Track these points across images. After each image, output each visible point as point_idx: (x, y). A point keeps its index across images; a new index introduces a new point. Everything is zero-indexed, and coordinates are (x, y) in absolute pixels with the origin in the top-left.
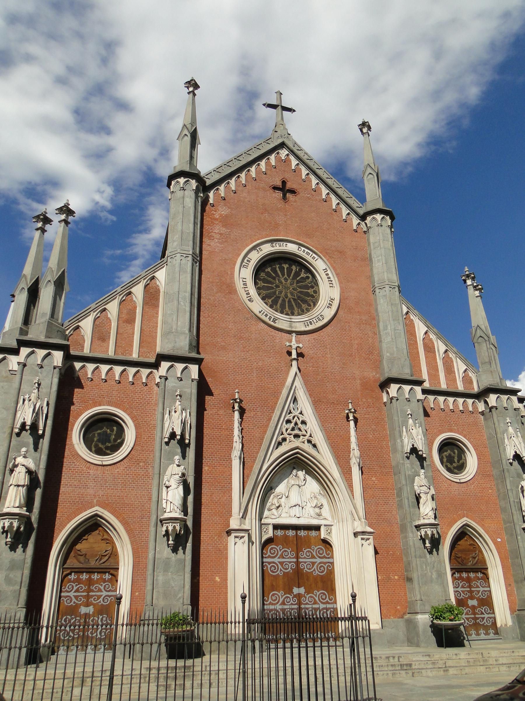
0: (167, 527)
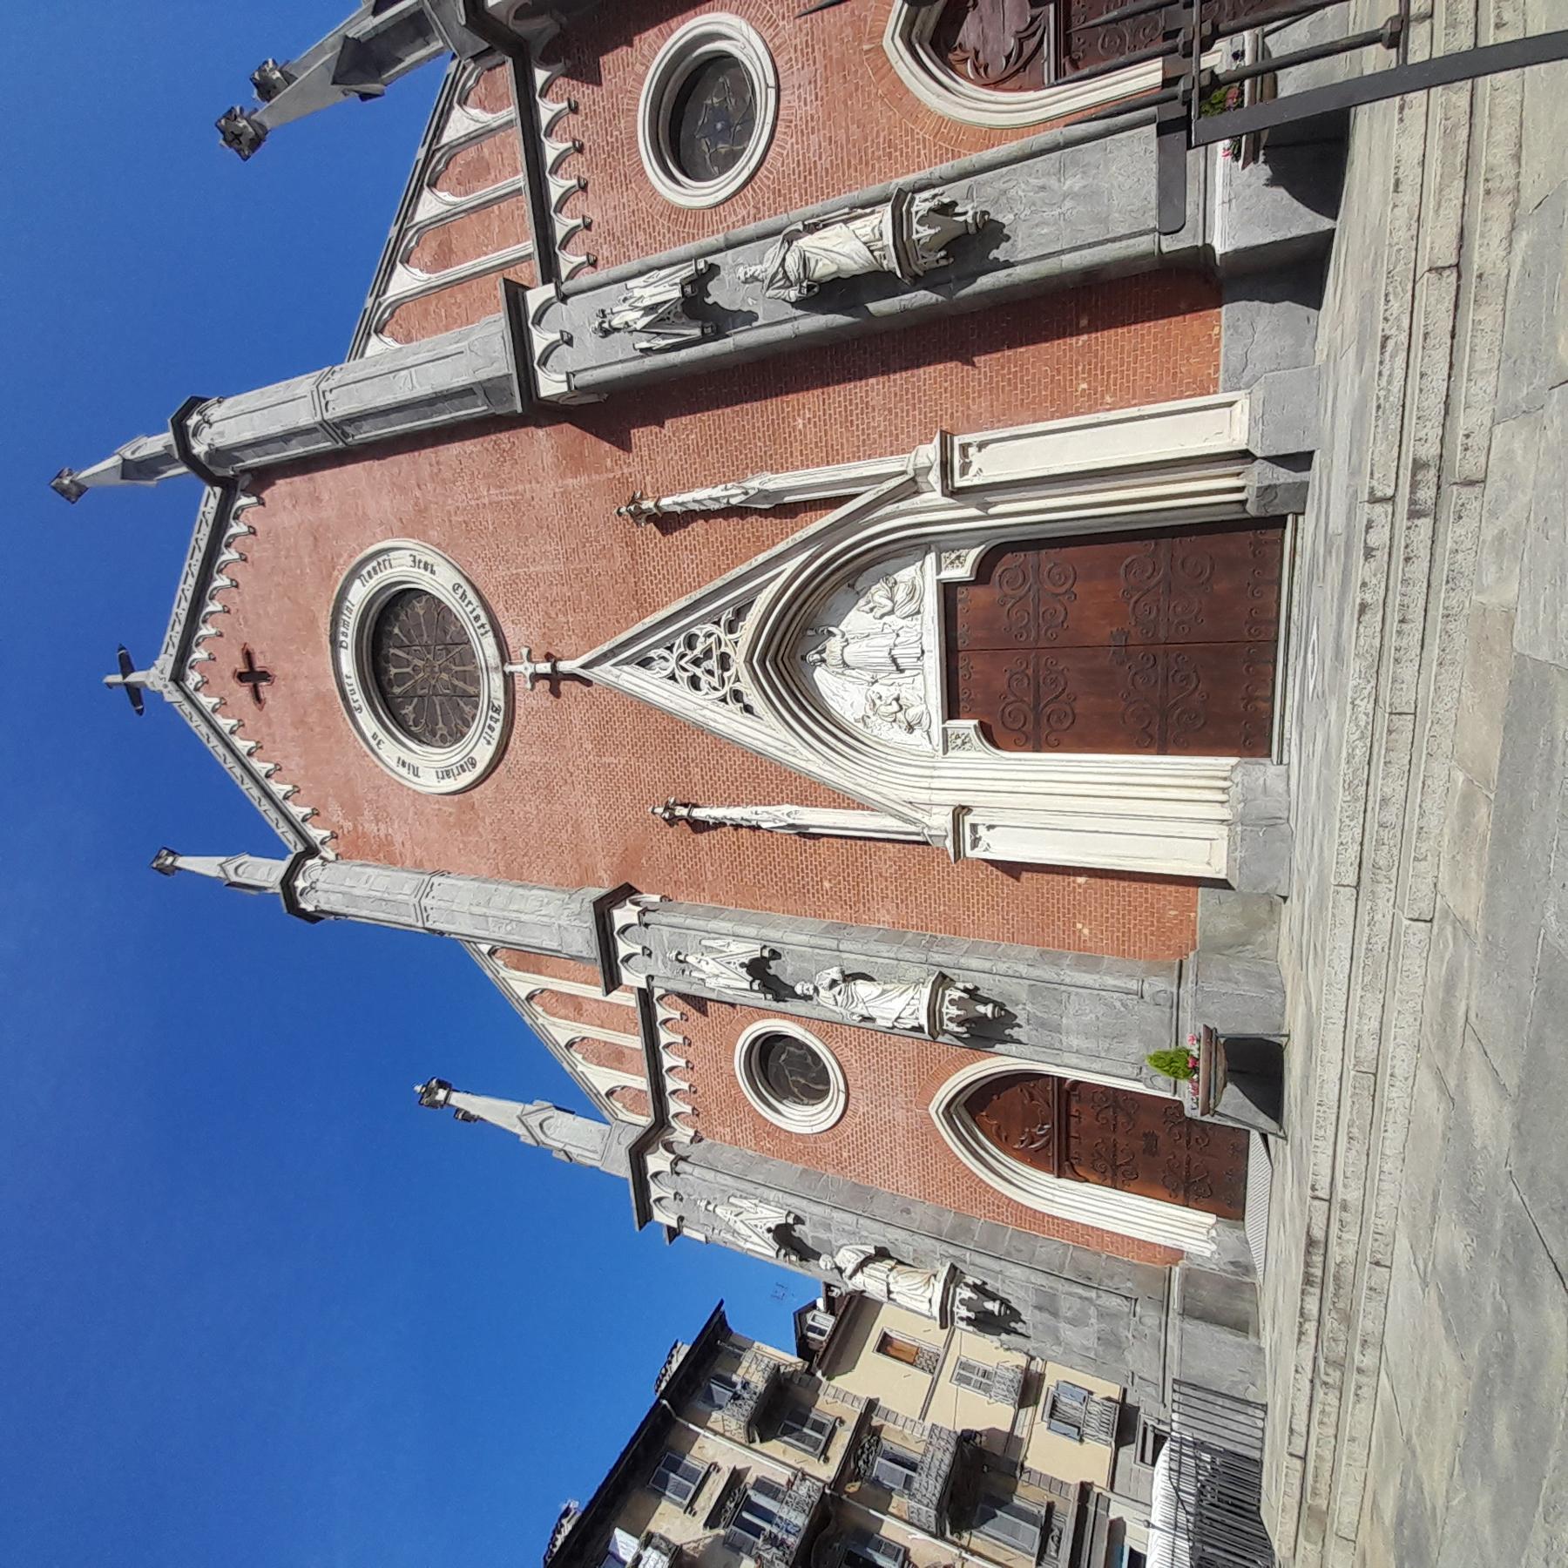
0: (951, 1019)
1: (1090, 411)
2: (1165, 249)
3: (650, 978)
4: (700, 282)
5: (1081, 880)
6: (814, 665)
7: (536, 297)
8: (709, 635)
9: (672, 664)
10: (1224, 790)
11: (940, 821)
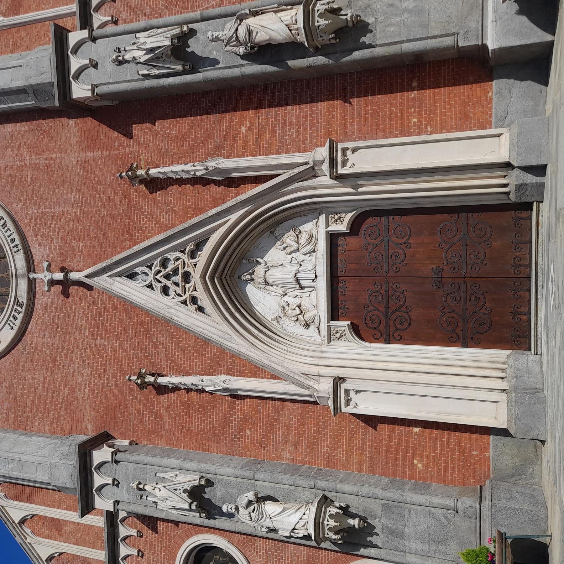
0: (330, 529)
1: (419, 134)
2: (460, 45)
3: (116, 503)
4: (184, 38)
5: (416, 430)
6: (246, 282)
7: (74, 37)
8: (178, 259)
9: (150, 278)
10: (503, 370)
11: (324, 388)
